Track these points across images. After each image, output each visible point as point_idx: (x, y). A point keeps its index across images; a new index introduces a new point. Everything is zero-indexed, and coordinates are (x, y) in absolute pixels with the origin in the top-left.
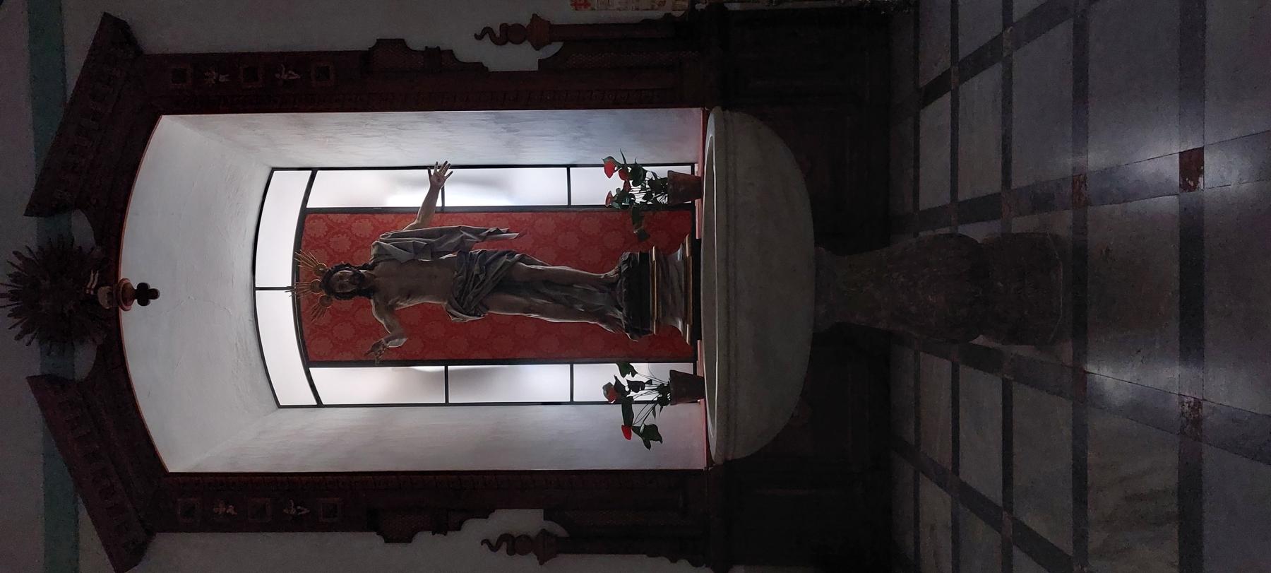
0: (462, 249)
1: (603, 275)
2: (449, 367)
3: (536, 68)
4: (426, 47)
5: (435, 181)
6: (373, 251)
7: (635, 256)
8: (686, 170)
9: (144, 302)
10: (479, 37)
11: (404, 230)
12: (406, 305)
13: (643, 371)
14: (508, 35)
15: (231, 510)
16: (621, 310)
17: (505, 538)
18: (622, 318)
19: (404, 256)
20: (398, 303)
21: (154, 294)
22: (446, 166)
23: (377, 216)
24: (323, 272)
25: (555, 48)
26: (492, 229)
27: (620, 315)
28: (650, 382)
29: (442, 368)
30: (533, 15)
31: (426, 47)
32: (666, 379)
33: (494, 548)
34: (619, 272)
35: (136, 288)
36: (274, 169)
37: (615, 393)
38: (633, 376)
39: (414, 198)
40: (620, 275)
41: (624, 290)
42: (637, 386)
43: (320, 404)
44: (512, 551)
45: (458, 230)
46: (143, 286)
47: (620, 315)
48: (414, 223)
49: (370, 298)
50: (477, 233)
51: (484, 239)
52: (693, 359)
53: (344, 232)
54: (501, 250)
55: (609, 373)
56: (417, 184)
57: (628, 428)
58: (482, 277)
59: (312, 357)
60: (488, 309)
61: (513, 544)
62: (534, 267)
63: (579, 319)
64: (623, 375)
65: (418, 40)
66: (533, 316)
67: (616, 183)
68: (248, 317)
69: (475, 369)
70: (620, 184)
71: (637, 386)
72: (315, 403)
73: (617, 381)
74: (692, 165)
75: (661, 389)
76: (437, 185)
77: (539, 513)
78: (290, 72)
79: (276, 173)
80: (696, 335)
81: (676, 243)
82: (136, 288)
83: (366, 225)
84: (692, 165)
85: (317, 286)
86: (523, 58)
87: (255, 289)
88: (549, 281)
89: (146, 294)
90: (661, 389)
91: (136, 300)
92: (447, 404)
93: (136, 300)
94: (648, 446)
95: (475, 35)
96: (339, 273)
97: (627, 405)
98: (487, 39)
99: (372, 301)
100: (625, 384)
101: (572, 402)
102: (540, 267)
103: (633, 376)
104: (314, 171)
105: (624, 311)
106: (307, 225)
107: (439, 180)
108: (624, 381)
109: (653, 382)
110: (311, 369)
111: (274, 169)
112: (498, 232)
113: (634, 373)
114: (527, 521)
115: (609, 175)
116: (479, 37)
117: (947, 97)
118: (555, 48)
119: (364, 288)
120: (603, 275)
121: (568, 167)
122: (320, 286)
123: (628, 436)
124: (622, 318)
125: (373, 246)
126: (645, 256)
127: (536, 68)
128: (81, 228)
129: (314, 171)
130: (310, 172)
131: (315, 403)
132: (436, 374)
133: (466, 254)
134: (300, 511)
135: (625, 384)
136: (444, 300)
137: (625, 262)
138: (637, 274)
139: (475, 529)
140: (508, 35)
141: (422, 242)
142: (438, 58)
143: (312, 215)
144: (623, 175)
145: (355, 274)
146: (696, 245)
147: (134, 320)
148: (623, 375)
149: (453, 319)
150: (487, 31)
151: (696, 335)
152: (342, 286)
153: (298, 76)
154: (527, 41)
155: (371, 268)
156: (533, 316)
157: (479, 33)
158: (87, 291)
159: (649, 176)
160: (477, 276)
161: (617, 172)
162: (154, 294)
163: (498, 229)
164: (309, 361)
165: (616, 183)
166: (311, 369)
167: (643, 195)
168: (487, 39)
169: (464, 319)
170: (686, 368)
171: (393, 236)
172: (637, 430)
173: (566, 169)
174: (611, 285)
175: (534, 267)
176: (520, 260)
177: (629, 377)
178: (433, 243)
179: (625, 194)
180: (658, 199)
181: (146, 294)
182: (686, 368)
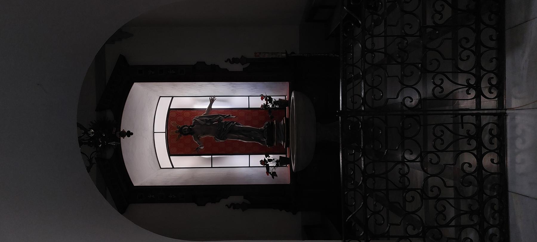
0: (219, 121)
1: (260, 128)
2: (213, 156)
3: (242, 70)
4: (211, 64)
5: (211, 101)
6: (193, 122)
7: (270, 123)
8: (283, 98)
9: (129, 136)
10: (226, 61)
11: (202, 115)
12: (203, 137)
13: (271, 157)
14: (234, 61)
15: (153, 196)
16: (265, 139)
17: (232, 204)
18: (265, 141)
19: (203, 123)
20: (201, 136)
21: (132, 134)
22: (215, 96)
23: (191, 111)
24: (179, 127)
25: (248, 64)
26: (228, 115)
27: (265, 140)
28: (274, 160)
29: (211, 156)
30: (242, 56)
31: (211, 64)
32: (278, 158)
33: (229, 207)
34: (265, 127)
35: (126, 132)
36: (160, 97)
37: (263, 162)
38: (269, 158)
39: (206, 106)
40: (265, 128)
41: (266, 133)
42: (270, 160)
43: (173, 168)
44: (234, 208)
45: (218, 116)
46: (129, 132)
47: (265, 140)
48: (205, 113)
49: (192, 135)
50: (223, 116)
51: (225, 118)
52: (286, 154)
53: (181, 116)
54: (230, 121)
55: (262, 157)
56: (205, 101)
57: (268, 172)
58: (225, 129)
59: (171, 153)
60: (227, 138)
61: (234, 206)
62: (240, 126)
63: (253, 141)
64: (266, 157)
65: (209, 62)
66: (240, 140)
67: (264, 102)
68: (152, 141)
69: (220, 157)
70: (265, 102)
71: (270, 160)
72: (172, 167)
73: (265, 159)
74: (285, 96)
75: (277, 161)
76: (212, 101)
77: (243, 197)
78: (173, 71)
79: (161, 98)
80: (287, 145)
81: (281, 119)
82: (126, 132)
83: (188, 113)
84: (285, 96)
85: (177, 132)
86: (238, 68)
87: (154, 133)
88: (244, 130)
89: (129, 134)
90: (277, 161)
91: (126, 136)
92: (212, 167)
93: (126, 136)
94: (273, 178)
95: (225, 61)
96: (184, 128)
97: (268, 167)
98: (228, 62)
99: (193, 136)
100: (267, 160)
101: (249, 167)
102: (241, 126)
103: (269, 158)
104: (173, 97)
105: (266, 139)
106: (170, 114)
107: (212, 101)
108: (267, 159)
109: (275, 159)
110: (171, 157)
111: (160, 97)
112: (229, 116)
113: (269, 157)
114: (238, 199)
115: (262, 99)
116: (226, 61)
117: (352, 83)
118: (248, 64)
119: (191, 132)
120: (260, 128)
121: (249, 96)
122: (178, 132)
123: (268, 175)
124: (265, 141)
125: (193, 120)
126: (273, 123)
127: (242, 70)
128: (110, 115)
129: (173, 97)
130: (171, 98)
131: (172, 167)
132: (210, 158)
133: (220, 122)
134: (173, 196)
135: (267, 160)
136: (214, 136)
137: (266, 125)
138: (270, 126)
139: (224, 202)
140: (234, 61)
141: (208, 119)
142: (215, 67)
143: (172, 111)
144: (266, 100)
145: (189, 128)
146: (287, 120)
147: (124, 141)
148: (266, 157)
149: (216, 141)
150: (229, 60)
151: (288, 145)
152: (185, 132)
153: (174, 72)
154: (239, 63)
155: (193, 126)
156: (240, 140)
157: (226, 60)
158: (113, 133)
159: (273, 100)
160: (224, 128)
161: (264, 99)
162: (132, 134)
163: (229, 115)
164: (170, 154)
165: (264, 102)
166: (171, 157)
167: (271, 106)
168: (228, 62)
169: (220, 141)
170: (284, 156)
171: (199, 117)
172: (270, 173)
173: (248, 97)
174: (262, 131)
175: (240, 126)
176: (236, 124)
177: (268, 158)
178: (211, 119)
179: (265, 106)
180: (276, 106)
181: (129, 134)
182: (284, 156)
